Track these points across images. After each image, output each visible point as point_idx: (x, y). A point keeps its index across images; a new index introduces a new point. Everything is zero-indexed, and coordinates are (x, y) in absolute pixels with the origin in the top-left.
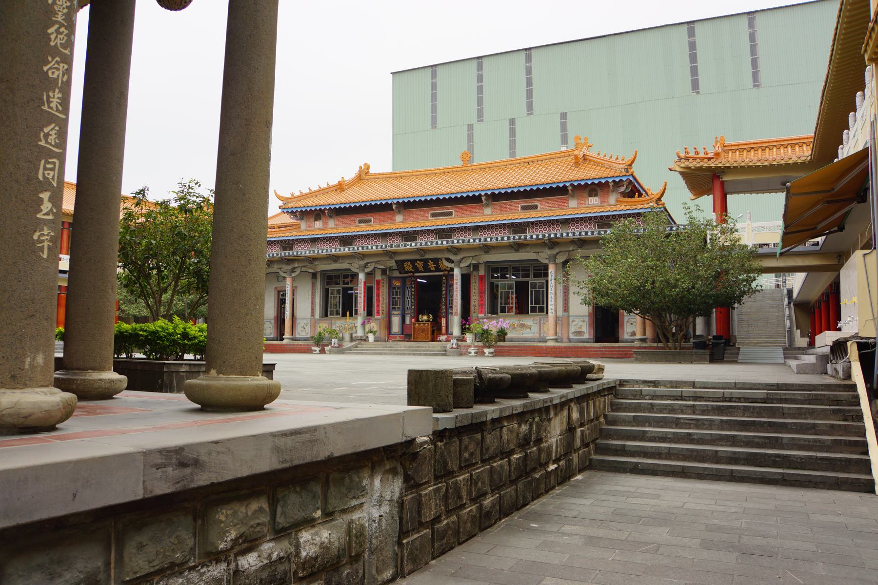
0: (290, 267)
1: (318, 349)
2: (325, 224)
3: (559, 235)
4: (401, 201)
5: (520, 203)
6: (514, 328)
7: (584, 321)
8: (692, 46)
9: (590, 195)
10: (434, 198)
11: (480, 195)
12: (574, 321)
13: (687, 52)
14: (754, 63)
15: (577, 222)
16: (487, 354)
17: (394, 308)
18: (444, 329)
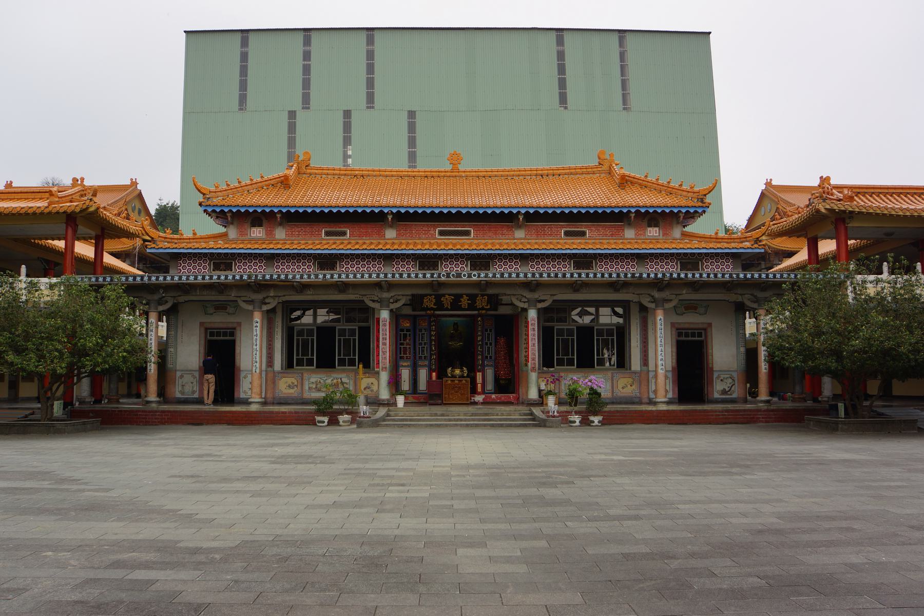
1: (326, 419)
2: (270, 233)
4: (284, 210)
8: (561, 56)
9: (253, 225)
10: (454, 211)
12: (182, 377)
13: (555, 62)
14: (624, 84)
15: (374, 259)
16: (596, 423)
17: (401, 358)
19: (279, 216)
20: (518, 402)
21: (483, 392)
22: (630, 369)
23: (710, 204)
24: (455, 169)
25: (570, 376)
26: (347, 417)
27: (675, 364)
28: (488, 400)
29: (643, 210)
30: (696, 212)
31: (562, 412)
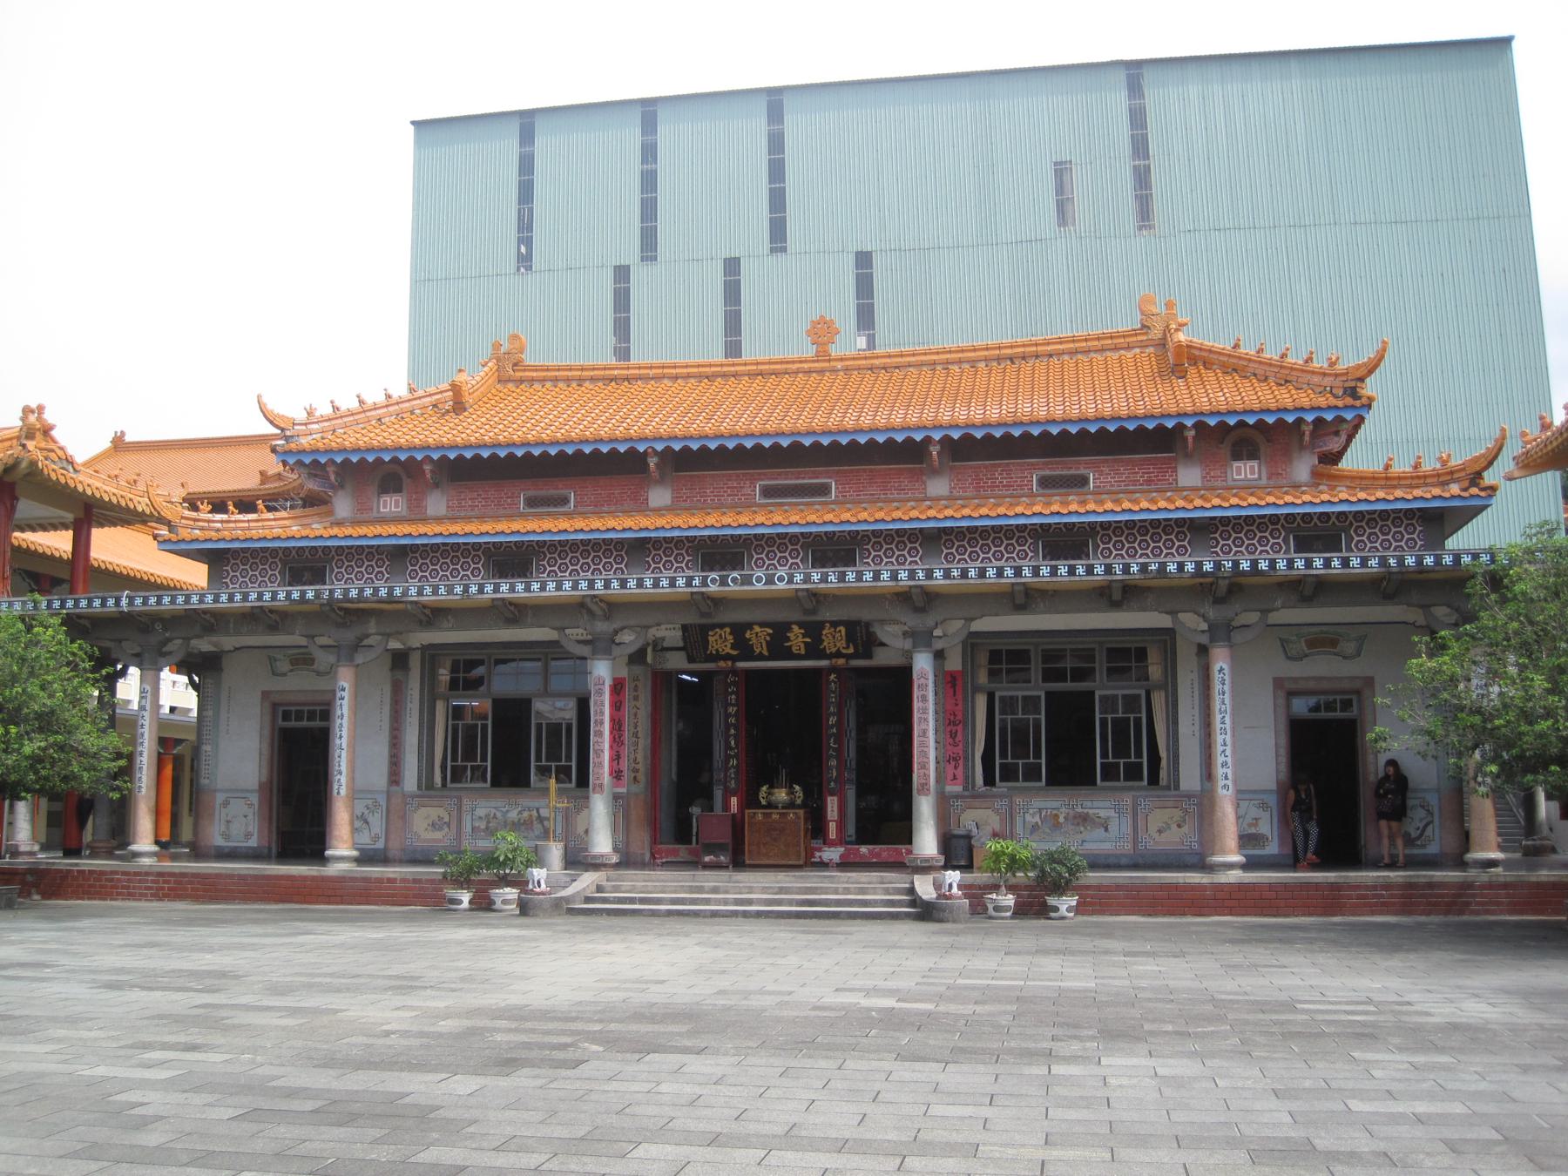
0: (349, 636)
3: (1263, 565)
5: (1033, 472)
6: (1057, 826)
7: (1264, 806)
9: (1237, 456)
11: (928, 440)
12: (226, 804)
18: (832, 827)
19: (427, 468)
20: (898, 865)
21: (841, 841)
22: (1177, 787)
23: (1371, 399)
24: (823, 355)
25: (1038, 803)
26: (511, 893)
27: (1284, 775)
28: (852, 859)
29: (1212, 422)
30: (1340, 420)
31: (970, 887)
